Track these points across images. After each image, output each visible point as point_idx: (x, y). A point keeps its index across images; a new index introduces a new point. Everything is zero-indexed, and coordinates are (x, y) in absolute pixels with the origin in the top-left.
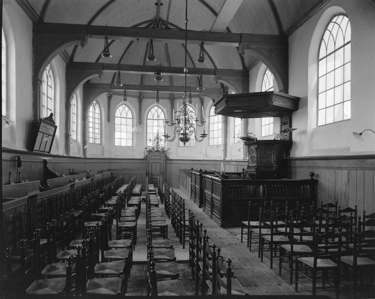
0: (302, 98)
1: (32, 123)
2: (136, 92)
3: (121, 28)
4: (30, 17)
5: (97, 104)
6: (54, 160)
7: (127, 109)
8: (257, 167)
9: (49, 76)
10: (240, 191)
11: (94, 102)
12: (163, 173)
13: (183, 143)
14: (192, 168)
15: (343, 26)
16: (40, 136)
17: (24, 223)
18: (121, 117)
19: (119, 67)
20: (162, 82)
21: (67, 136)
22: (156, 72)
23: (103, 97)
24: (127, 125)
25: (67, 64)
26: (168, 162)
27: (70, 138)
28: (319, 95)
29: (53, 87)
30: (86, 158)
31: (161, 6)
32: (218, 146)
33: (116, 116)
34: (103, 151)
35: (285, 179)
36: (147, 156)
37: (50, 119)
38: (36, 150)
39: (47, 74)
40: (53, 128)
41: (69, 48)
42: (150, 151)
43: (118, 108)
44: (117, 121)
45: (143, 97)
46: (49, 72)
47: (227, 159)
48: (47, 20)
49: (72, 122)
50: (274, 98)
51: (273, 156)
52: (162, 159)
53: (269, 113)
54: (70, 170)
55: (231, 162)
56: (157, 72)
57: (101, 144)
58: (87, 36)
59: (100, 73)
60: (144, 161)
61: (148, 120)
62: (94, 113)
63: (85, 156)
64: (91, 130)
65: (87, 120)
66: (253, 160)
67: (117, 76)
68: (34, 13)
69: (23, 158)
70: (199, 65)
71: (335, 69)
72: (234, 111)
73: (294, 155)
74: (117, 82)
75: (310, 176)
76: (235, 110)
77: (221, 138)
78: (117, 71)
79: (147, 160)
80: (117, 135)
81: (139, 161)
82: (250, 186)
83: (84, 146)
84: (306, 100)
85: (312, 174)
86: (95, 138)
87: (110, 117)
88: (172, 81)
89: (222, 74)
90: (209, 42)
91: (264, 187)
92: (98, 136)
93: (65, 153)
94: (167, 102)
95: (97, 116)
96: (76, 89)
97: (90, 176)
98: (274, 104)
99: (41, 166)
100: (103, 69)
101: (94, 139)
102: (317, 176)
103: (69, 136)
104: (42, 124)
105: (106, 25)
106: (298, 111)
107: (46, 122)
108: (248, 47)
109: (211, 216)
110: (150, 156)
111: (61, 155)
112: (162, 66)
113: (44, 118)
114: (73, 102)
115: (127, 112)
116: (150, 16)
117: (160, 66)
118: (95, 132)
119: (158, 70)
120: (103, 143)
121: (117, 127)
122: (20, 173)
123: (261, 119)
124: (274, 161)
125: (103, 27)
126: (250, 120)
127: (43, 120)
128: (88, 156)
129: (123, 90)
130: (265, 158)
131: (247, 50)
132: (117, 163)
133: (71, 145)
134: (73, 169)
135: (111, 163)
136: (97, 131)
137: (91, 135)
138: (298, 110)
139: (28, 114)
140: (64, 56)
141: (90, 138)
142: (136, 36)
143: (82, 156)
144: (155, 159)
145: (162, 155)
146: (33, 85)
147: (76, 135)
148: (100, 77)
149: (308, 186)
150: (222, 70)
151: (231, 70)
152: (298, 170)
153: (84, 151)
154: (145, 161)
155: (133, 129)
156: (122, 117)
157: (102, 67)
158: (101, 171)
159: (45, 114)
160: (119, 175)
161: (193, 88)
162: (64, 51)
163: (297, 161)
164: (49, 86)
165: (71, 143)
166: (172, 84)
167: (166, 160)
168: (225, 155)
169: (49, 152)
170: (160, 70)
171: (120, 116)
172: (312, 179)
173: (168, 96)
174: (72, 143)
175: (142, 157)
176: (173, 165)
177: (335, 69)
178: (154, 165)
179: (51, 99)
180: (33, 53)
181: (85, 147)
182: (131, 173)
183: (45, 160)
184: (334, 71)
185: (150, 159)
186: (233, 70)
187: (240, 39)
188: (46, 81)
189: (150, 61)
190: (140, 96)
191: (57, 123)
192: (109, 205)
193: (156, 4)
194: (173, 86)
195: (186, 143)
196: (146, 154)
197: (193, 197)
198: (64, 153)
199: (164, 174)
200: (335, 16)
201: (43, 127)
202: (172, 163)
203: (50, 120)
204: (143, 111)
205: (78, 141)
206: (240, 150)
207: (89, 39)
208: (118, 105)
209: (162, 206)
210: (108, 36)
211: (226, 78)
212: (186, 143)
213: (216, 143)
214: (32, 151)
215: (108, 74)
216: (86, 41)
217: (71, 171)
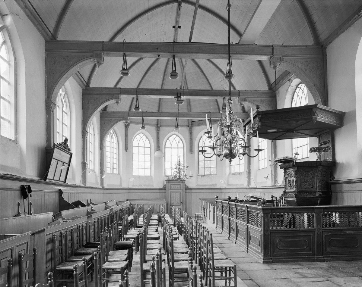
0: (348, 112)
1: (46, 149)
2: (73, 259)
3: (141, 43)
4: (42, 35)
5: (115, 133)
6: (70, 190)
7: (144, 138)
8: (298, 192)
9: (65, 101)
10: (277, 221)
11: (111, 131)
12: (182, 203)
13: (229, 160)
14: (217, 196)
15: (302, 88)
16: (53, 162)
17: (26, 268)
18: (139, 147)
19: (137, 91)
20: (183, 107)
21: (84, 165)
22: (176, 95)
23: (120, 126)
24: (145, 154)
25: (83, 90)
26: (187, 191)
27: (87, 167)
29: (69, 113)
30: (104, 189)
31: (179, 29)
32: (240, 174)
33: (133, 145)
34: (121, 180)
35: (335, 206)
36: (165, 185)
37: (64, 144)
38: (49, 178)
39: (62, 99)
40: (69, 156)
41: (85, 67)
42: (168, 181)
43: (135, 137)
44: (135, 150)
45: (161, 126)
46: (64, 97)
47: (251, 187)
48: (61, 37)
49: (89, 161)
50: (318, 112)
51: (315, 180)
52: (181, 188)
53: (306, 132)
54: (87, 200)
55: (257, 189)
56: (177, 95)
57: (119, 174)
58: (103, 53)
59: (118, 98)
60: (163, 191)
61: (166, 149)
62: (112, 143)
63: (103, 186)
64: (108, 160)
65: (104, 150)
66: (292, 185)
67: (135, 102)
68: (47, 29)
69: (33, 187)
72: (269, 131)
73: (339, 179)
74: (136, 107)
76: (269, 130)
77: (243, 165)
78: (135, 96)
79: (166, 189)
80: (135, 164)
81: (158, 191)
82: (358, 213)
83: (101, 176)
84: (353, 114)
86: (112, 168)
88: (190, 108)
89: (246, 95)
90: (237, 56)
91: (309, 217)
92: (116, 166)
93: (82, 183)
94: (184, 130)
95: (115, 146)
96: (93, 116)
97: (109, 206)
98: (318, 120)
99: (55, 197)
100: (121, 93)
101: (112, 170)
103: (86, 165)
104: (56, 150)
105: (124, 41)
106: (343, 128)
107: (60, 148)
108: (281, 60)
109: (247, 249)
110: (169, 186)
111: (78, 185)
112: (182, 88)
113: (58, 144)
114: (90, 130)
115: (144, 141)
117: (181, 88)
118: (113, 162)
119: (178, 94)
120: (121, 173)
121: (135, 157)
122: (31, 204)
123: (292, 141)
124: (317, 185)
125: (121, 43)
126: (279, 142)
127: (56, 146)
128: (106, 186)
129: (141, 118)
130: (306, 182)
131: (279, 63)
132: (137, 193)
133: (88, 175)
134: (91, 200)
135: (130, 193)
136: (115, 161)
137: (109, 165)
138: (343, 127)
139: (40, 141)
140: (79, 76)
141: (107, 167)
142: (157, 52)
143: (100, 187)
144: (174, 188)
145: (181, 184)
146: (46, 108)
147: (93, 164)
148: (117, 102)
149: (360, 213)
150: (246, 92)
151: (256, 91)
152: (346, 195)
153: (102, 181)
154: (163, 190)
155: (155, 154)
156: (139, 146)
157: (119, 93)
158: (120, 201)
159: (59, 140)
160: (138, 205)
161: (213, 113)
162: (78, 73)
163: (345, 185)
164: (64, 112)
165: (88, 172)
166: (190, 110)
167: (185, 189)
168: (249, 182)
169: (65, 182)
170: (180, 93)
171: (138, 146)
173: (186, 124)
174: (89, 172)
175: (161, 186)
176: (192, 194)
178: (173, 194)
179: (66, 126)
180: (46, 74)
181: (102, 178)
182: (151, 203)
183: (60, 190)
185: (169, 188)
186: (259, 90)
187: (272, 52)
188: (61, 107)
189: (173, 79)
190: (157, 125)
191: (73, 151)
192: (128, 239)
193: (174, 27)
194: (192, 111)
195: (232, 160)
196: (165, 183)
198: (81, 183)
199: (184, 203)
201: (57, 154)
202: (192, 192)
203: (64, 146)
204: (160, 141)
205: (95, 170)
206: (267, 177)
207: (106, 58)
209: (182, 238)
210: (127, 53)
211: (251, 100)
212: (232, 160)
213: (237, 171)
214: (46, 180)
215: (126, 100)
216: (102, 59)
217: (89, 202)
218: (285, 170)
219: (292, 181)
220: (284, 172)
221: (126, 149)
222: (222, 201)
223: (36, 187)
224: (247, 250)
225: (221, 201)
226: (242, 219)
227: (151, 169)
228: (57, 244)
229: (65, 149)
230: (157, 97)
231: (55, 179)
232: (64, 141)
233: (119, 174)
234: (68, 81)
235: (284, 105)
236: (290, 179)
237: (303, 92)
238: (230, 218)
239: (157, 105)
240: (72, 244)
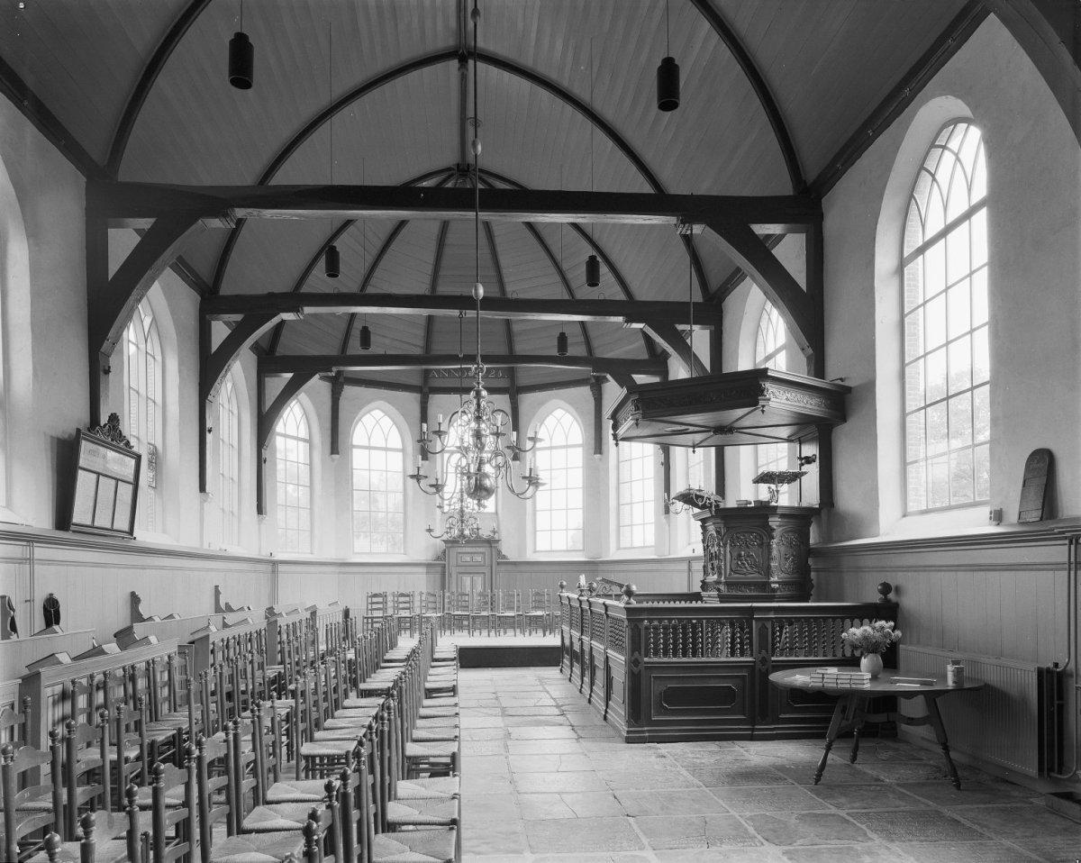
2: (411, 370)
23: (317, 385)
28: (908, 419)
29: (159, 358)
40: (133, 462)
57: (497, 513)
70: (585, 292)
71: (948, 343)
75: (881, 592)
85: (886, 588)
87: (336, 440)
102: (898, 590)
114: (677, 420)
116: (449, 158)
120: (499, 512)
172: (887, 601)
177: (948, 343)
184: (949, 284)
197: (566, 665)
200: (945, 126)
208: (361, 413)
221: (334, 449)
226: (600, 639)
228: (141, 683)
229: (114, 443)
230: (425, 312)
232: (108, 421)
233: (497, 513)
234: (156, 282)
235: (160, 283)
238: (583, 637)
239: (421, 332)
240: (316, 684)
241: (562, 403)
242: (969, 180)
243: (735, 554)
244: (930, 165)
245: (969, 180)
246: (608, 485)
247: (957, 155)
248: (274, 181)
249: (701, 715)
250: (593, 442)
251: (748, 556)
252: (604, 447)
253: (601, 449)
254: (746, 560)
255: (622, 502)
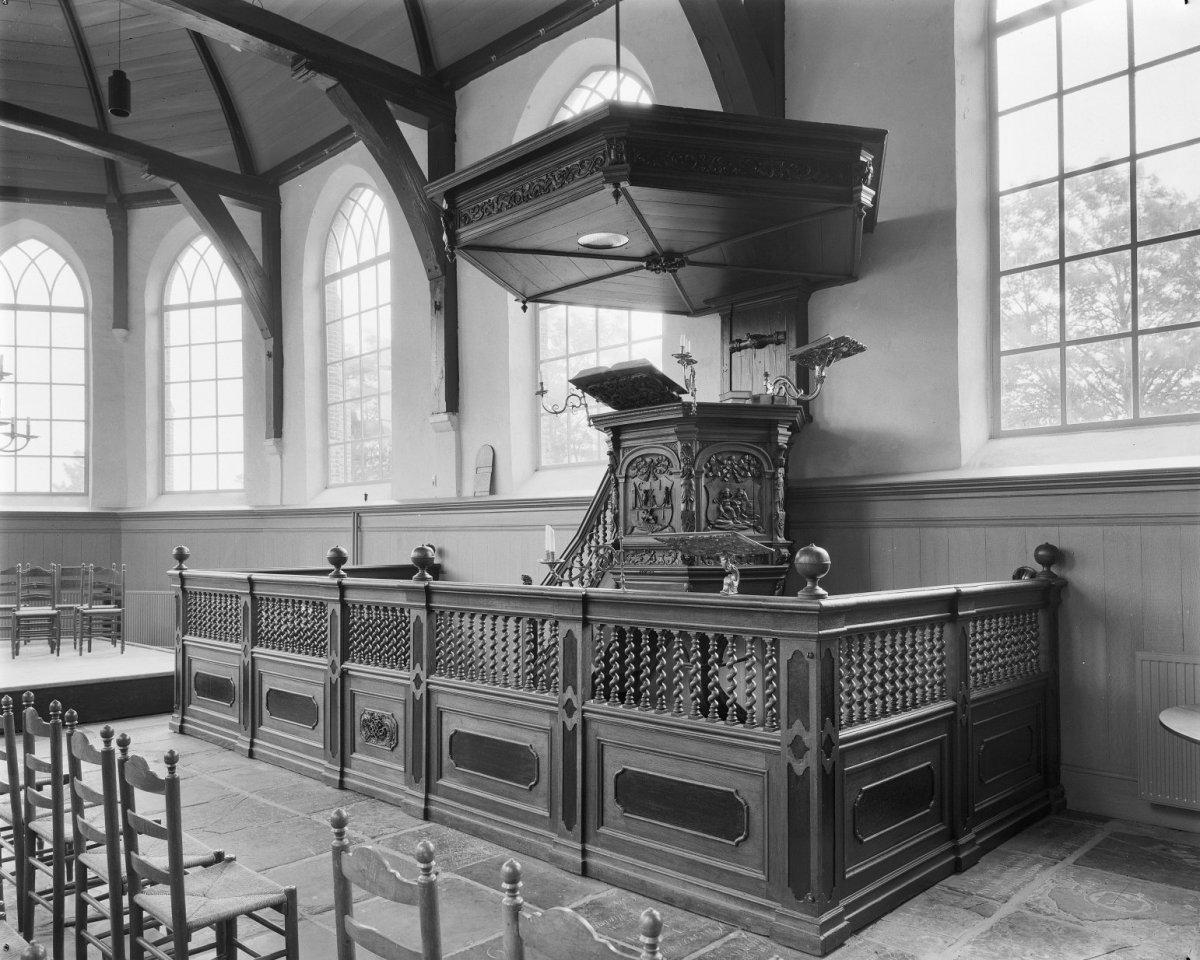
76: (585, 234)
218: (617, 434)
219: (660, 497)
220: (610, 453)
222: (255, 576)
223: (519, 734)
224: (579, 859)
225: (245, 576)
227: (51, 494)
231: (505, 493)
236: (646, 486)
237: (366, 216)
241: (39, 227)
242: (376, 232)
243: (714, 493)
244: (346, 211)
245: (376, 232)
246: (143, 384)
247: (366, 212)
248: (239, 951)
249: (897, 885)
250: (111, 308)
251: (736, 497)
252: (134, 319)
253: (126, 320)
254: (732, 504)
255: (331, 400)
